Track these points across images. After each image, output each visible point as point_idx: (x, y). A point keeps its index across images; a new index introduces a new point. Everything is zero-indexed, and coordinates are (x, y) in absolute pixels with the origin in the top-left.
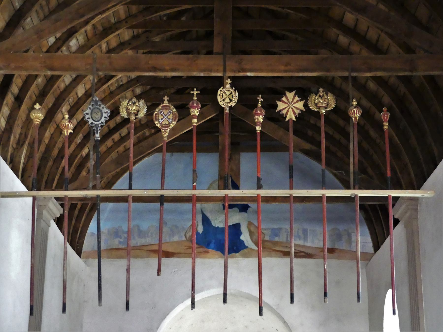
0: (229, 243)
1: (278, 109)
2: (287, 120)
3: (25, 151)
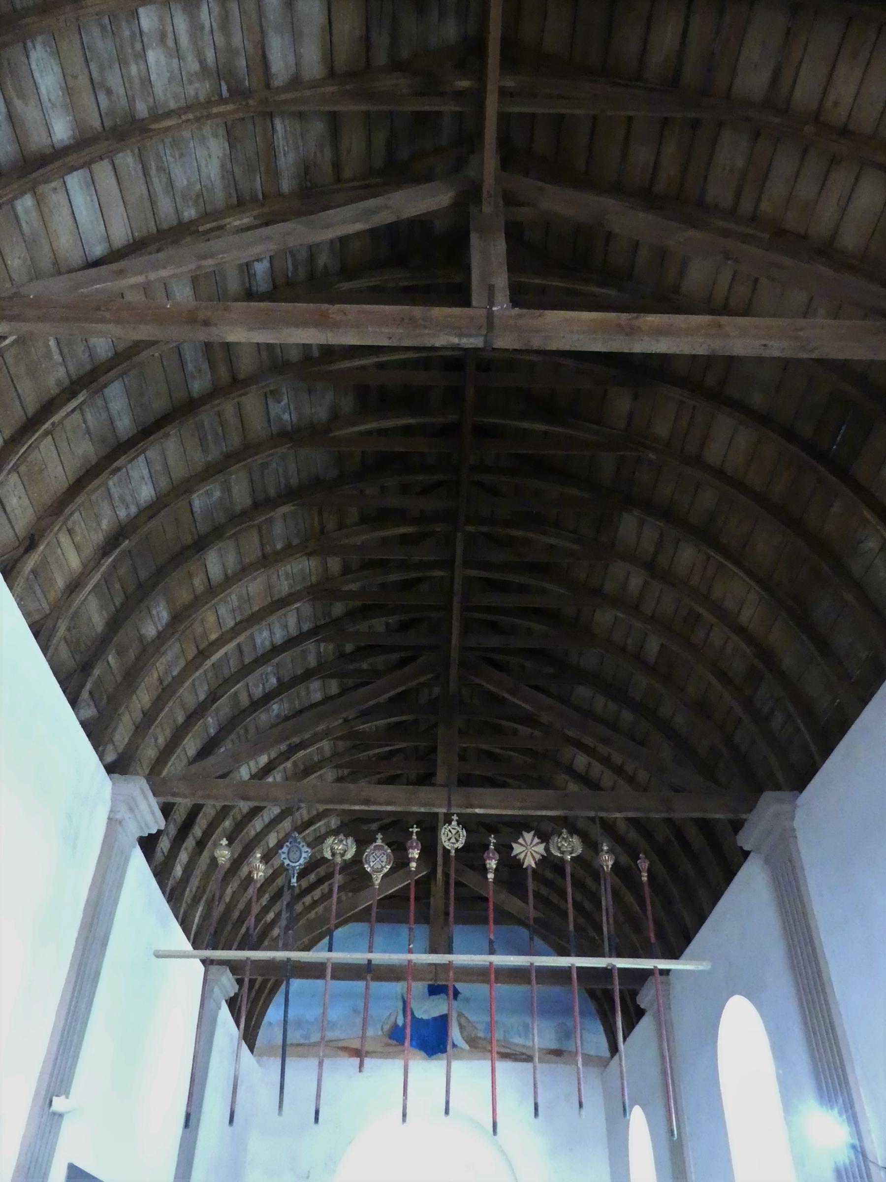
0: (433, 1040)
1: (514, 853)
2: (524, 867)
3: (200, 909)
